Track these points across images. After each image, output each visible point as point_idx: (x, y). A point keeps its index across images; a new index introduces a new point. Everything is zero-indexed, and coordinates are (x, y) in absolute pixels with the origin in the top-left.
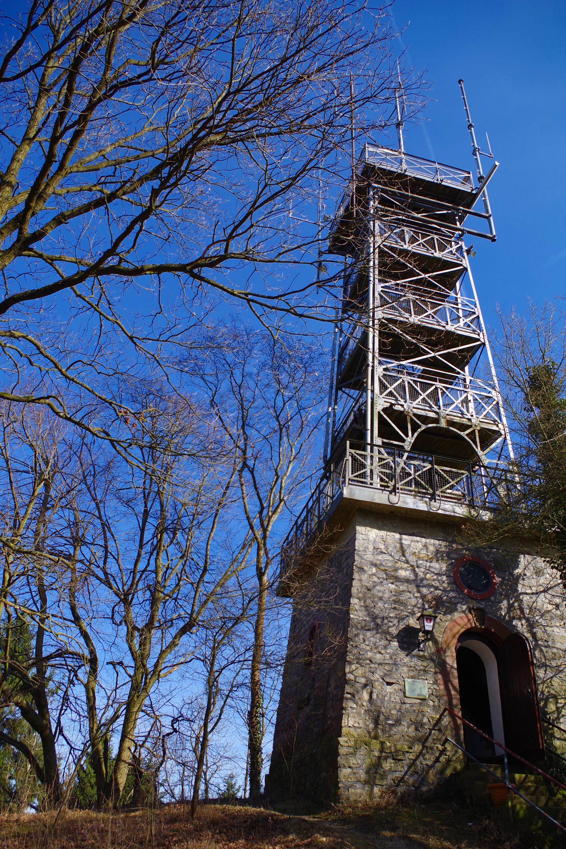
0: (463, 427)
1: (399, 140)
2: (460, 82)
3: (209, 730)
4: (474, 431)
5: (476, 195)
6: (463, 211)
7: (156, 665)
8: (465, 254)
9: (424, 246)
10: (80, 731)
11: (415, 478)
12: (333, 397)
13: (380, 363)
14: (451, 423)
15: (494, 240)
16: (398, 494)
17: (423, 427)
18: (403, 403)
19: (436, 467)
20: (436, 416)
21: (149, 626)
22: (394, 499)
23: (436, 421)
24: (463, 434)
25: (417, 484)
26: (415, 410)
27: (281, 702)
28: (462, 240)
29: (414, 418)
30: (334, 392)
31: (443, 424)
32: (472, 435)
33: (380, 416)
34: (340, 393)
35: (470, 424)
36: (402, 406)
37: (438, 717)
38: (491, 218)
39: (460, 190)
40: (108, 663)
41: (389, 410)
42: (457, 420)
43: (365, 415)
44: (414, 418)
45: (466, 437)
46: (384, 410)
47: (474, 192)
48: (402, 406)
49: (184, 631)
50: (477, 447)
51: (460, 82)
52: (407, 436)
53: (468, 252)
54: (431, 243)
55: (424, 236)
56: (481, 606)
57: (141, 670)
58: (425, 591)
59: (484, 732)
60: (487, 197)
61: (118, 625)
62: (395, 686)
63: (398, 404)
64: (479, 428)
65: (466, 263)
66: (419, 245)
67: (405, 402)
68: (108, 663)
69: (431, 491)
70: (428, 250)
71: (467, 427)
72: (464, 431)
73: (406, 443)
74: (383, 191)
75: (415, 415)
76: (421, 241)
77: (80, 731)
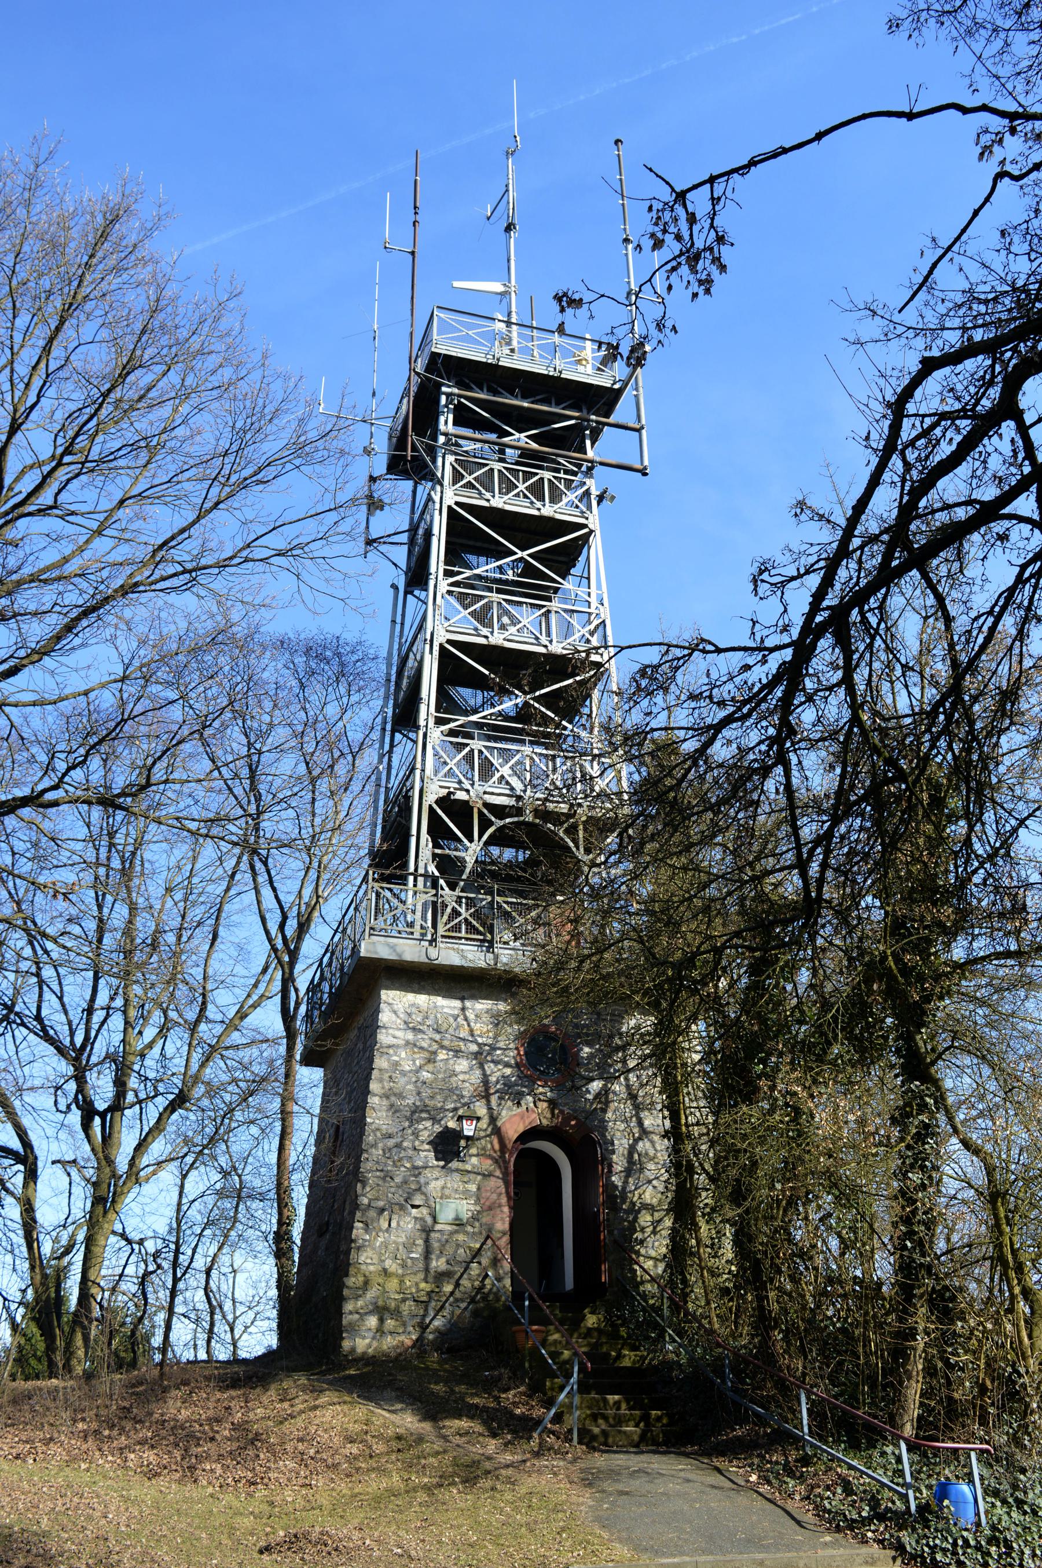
1: (509, 261)
2: (617, 142)
5: (619, 392)
6: (597, 422)
7: (132, 1163)
8: (594, 503)
9: (526, 496)
10: (14, 1270)
11: (466, 919)
13: (439, 722)
15: (645, 474)
18: (469, 787)
19: (498, 899)
21: (117, 1106)
22: (433, 953)
23: (519, 811)
26: (487, 797)
28: (591, 477)
29: (485, 811)
30: (388, 734)
31: (530, 818)
33: (431, 810)
34: (398, 736)
36: (468, 791)
37: (478, 1246)
38: (644, 432)
40: (54, 1162)
41: (445, 802)
43: (410, 809)
44: (485, 811)
46: (440, 801)
47: (616, 386)
48: (468, 791)
49: (172, 1107)
50: (578, 849)
51: (617, 142)
53: (601, 498)
54: (536, 489)
55: (528, 476)
57: (107, 1170)
58: (489, 1067)
60: (641, 390)
61: (65, 1113)
63: (462, 789)
64: (584, 818)
65: (593, 521)
66: (517, 495)
67: (472, 785)
68: (54, 1162)
69: (489, 937)
70: (532, 503)
73: (470, 851)
74: (460, 396)
75: (486, 805)
76: (522, 487)
77: (14, 1270)
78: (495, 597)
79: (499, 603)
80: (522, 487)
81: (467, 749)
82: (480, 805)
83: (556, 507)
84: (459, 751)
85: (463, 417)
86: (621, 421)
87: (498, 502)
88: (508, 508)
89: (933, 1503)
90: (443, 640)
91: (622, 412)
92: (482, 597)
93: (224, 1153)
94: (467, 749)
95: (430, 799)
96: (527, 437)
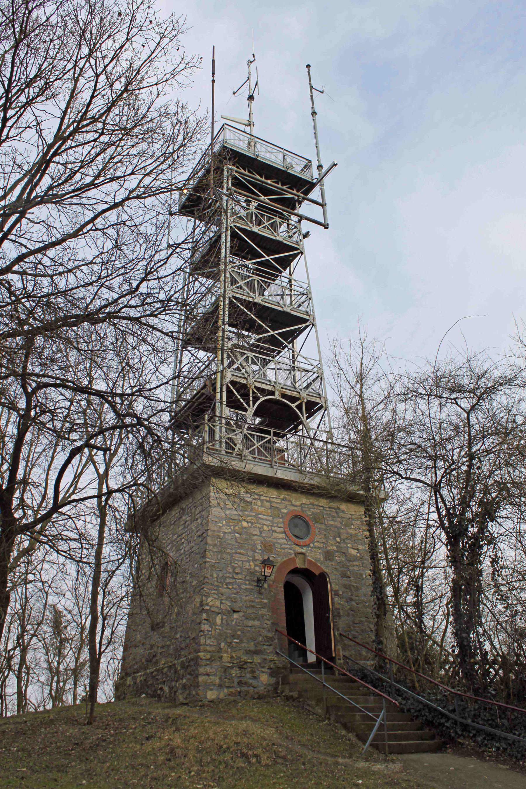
0: (293, 399)
3: (102, 650)
4: (301, 403)
9: (268, 229)
12: (72, 194)
14: (284, 396)
16: (245, 461)
17: (262, 399)
20: (273, 390)
23: (272, 393)
24: (293, 406)
25: (260, 453)
27: (12, 497)
31: (277, 396)
32: (299, 407)
35: (298, 396)
39: (301, 178)
42: (289, 393)
45: (295, 409)
52: (249, 406)
55: (269, 219)
56: (303, 551)
59: (299, 642)
62: (241, 614)
66: (264, 227)
69: (269, 458)
71: (297, 399)
72: (293, 403)
73: (248, 412)
76: (266, 224)
78: (256, 278)
79: (258, 281)
80: (266, 224)
81: (245, 356)
82: (253, 387)
83: (259, 228)
84: (242, 356)
85: (237, 183)
86: (315, 199)
87: (256, 229)
88: (260, 233)
89: (245, 449)
90: (230, 295)
91: (315, 194)
92: (251, 277)
93: (56, 298)
94: (245, 356)
95: (227, 380)
96: (268, 199)
